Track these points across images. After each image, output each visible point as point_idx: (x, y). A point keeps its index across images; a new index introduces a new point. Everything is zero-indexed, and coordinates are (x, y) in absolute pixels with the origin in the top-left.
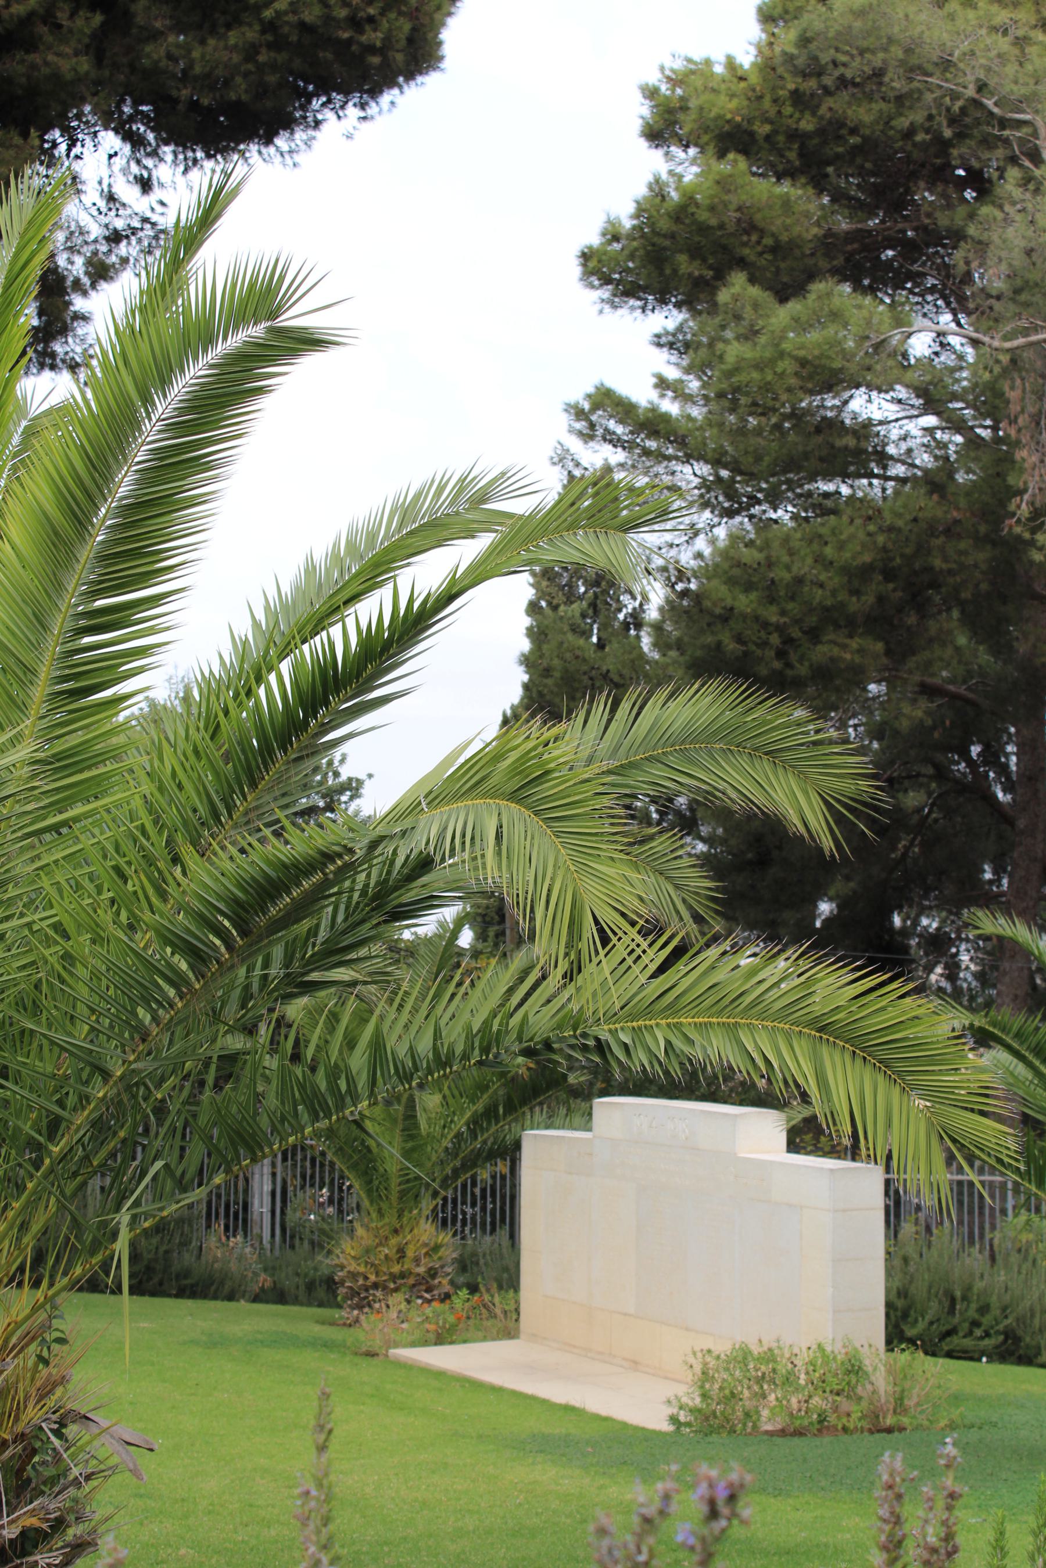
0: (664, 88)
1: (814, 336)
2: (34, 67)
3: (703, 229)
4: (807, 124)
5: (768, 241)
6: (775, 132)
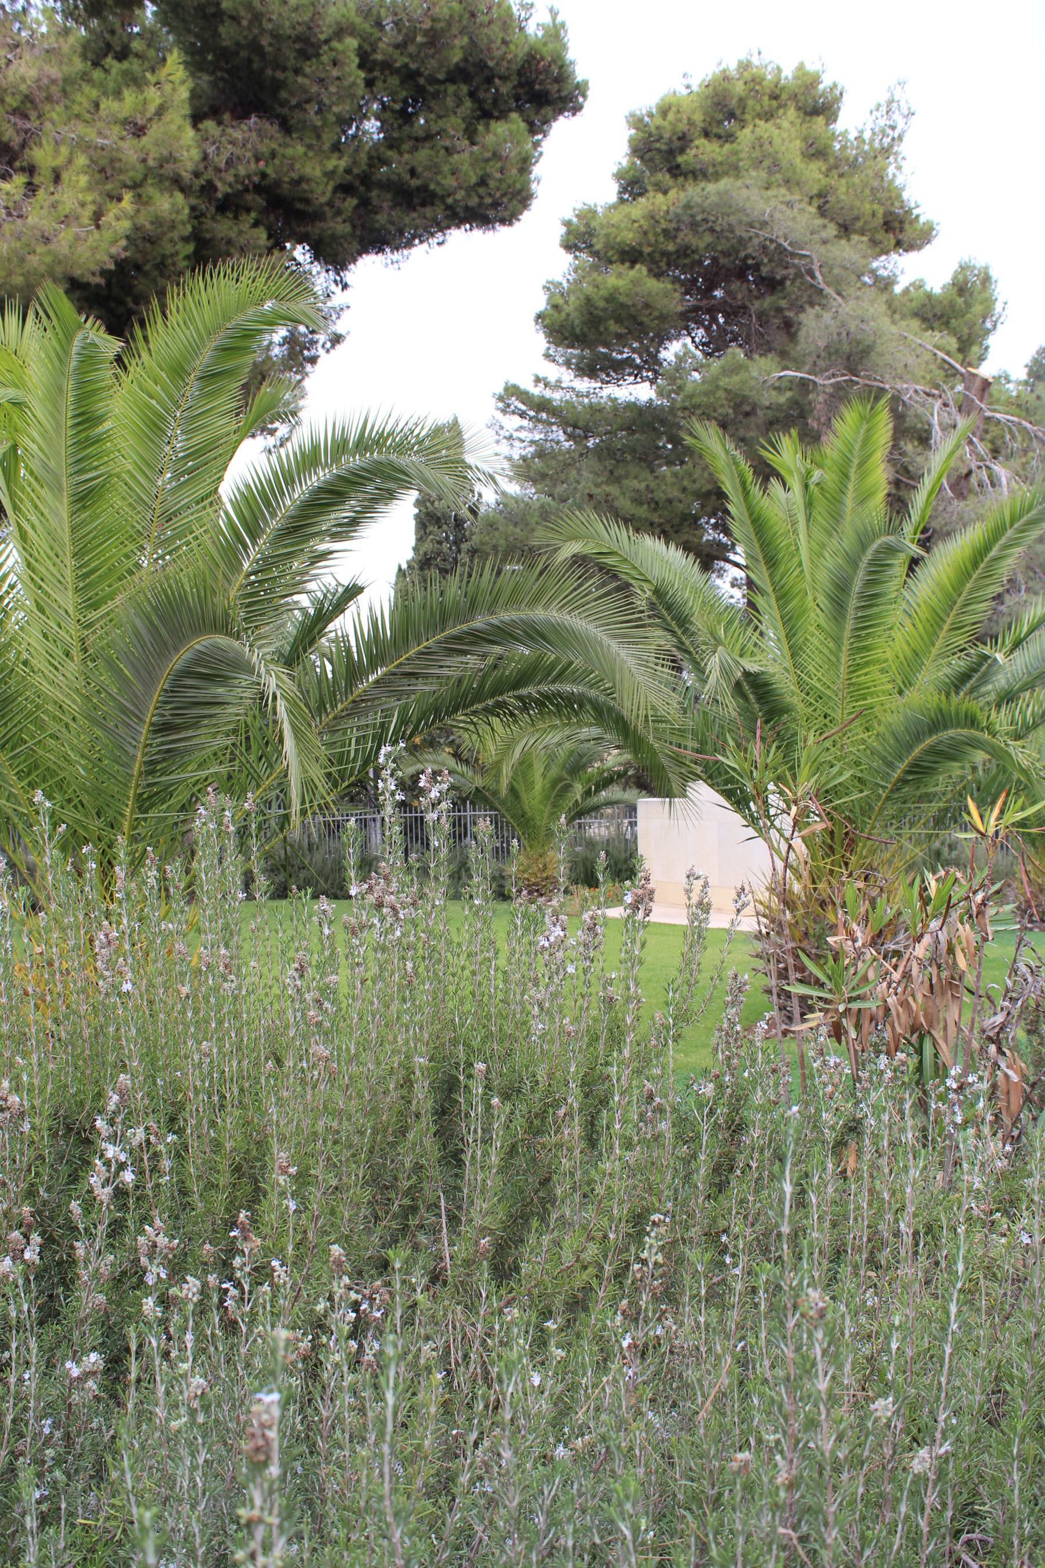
0: (575, 220)
1: (736, 379)
2: (323, 230)
3: (623, 306)
4: (671, 247)
5: (656, 313)
6: (654, 252)
